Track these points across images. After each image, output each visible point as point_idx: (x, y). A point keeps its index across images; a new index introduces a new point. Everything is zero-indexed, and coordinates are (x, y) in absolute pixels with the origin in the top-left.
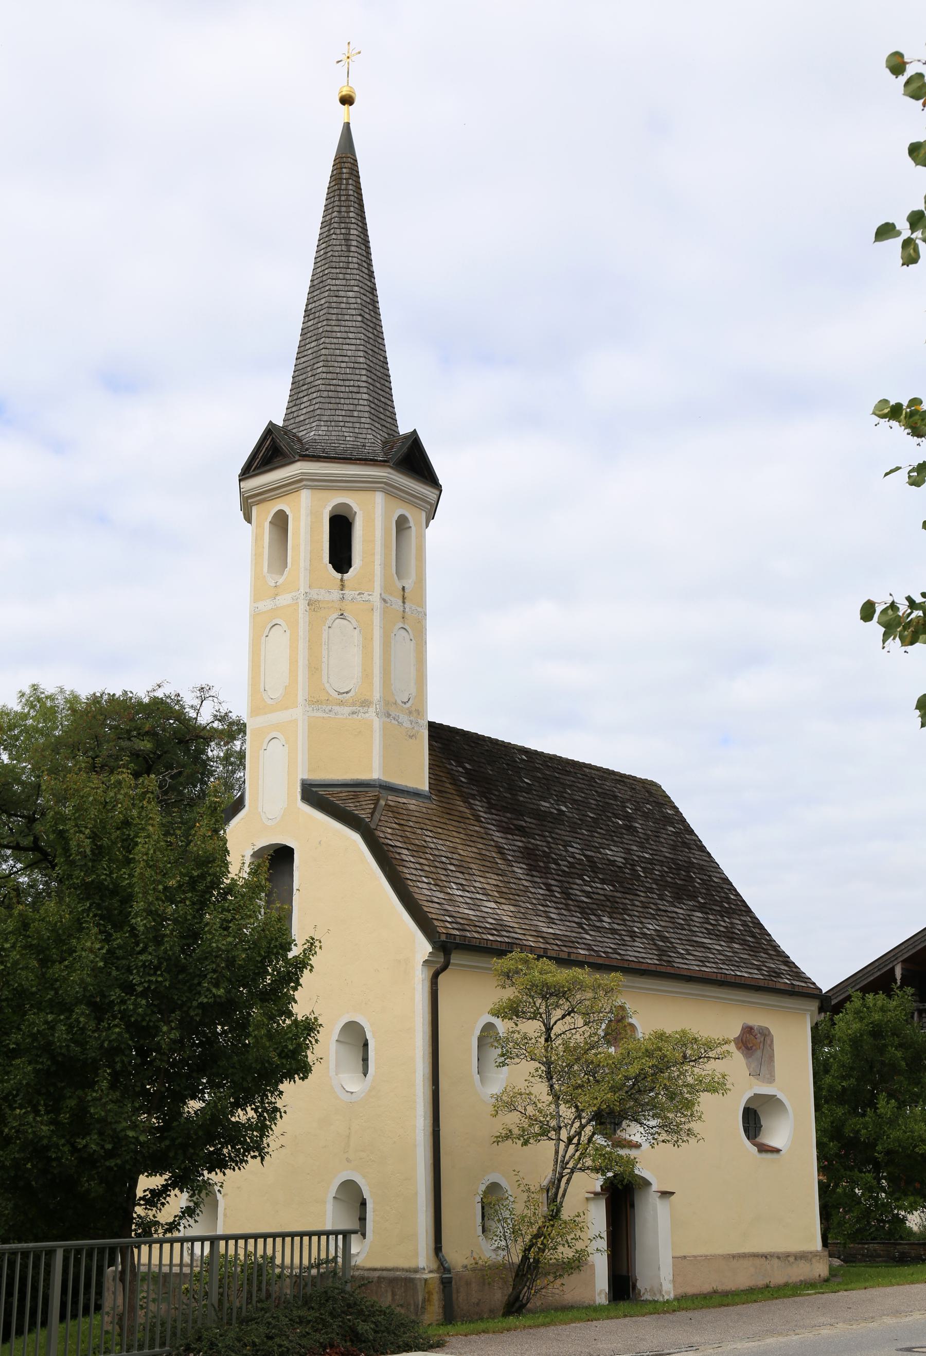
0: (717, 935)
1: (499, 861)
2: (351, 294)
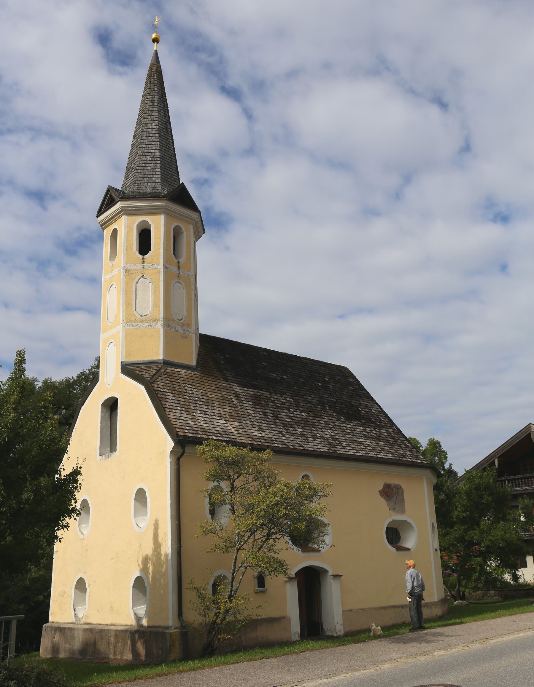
0: (369, 438)
1: (234, 400)
2: (153, 124)
